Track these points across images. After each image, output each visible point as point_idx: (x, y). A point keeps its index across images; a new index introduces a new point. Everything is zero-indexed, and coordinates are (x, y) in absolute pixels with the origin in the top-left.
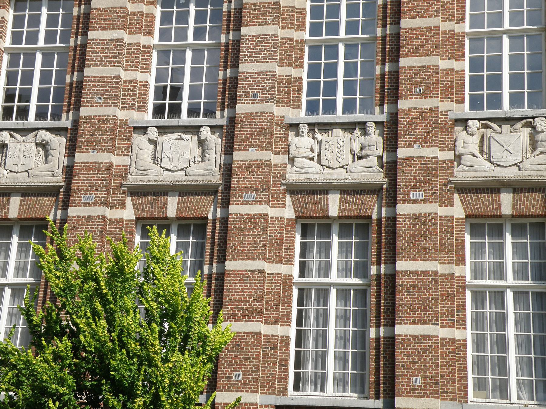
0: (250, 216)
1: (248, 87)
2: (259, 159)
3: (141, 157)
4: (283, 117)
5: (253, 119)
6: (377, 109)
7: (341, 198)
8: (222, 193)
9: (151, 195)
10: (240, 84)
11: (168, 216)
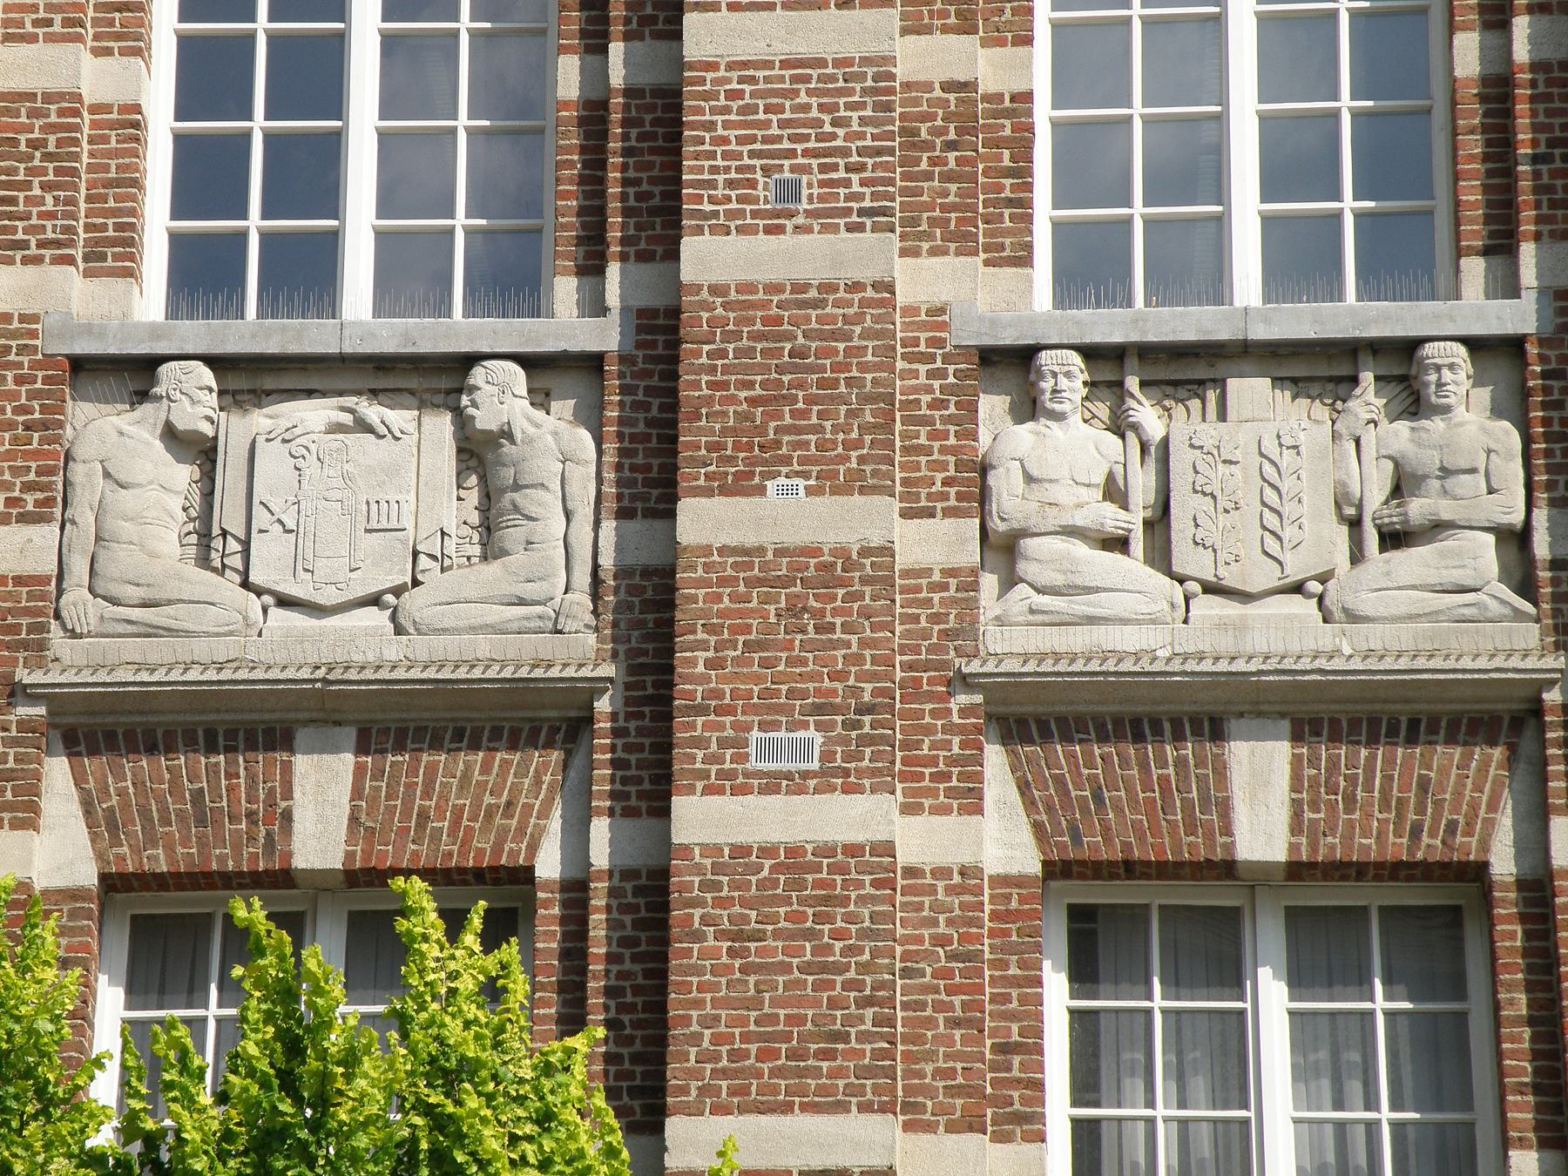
0: (794, 860)
1: (741, 140)
2: (830, 537)
3: (126, 529)
4: (941, 310)
5: (778, 321)
6: (1474, 269)
7: (1296, 761)
8: (616, 733)
9: (191, 744)
10: (694, 126)
11: (299, 862)
